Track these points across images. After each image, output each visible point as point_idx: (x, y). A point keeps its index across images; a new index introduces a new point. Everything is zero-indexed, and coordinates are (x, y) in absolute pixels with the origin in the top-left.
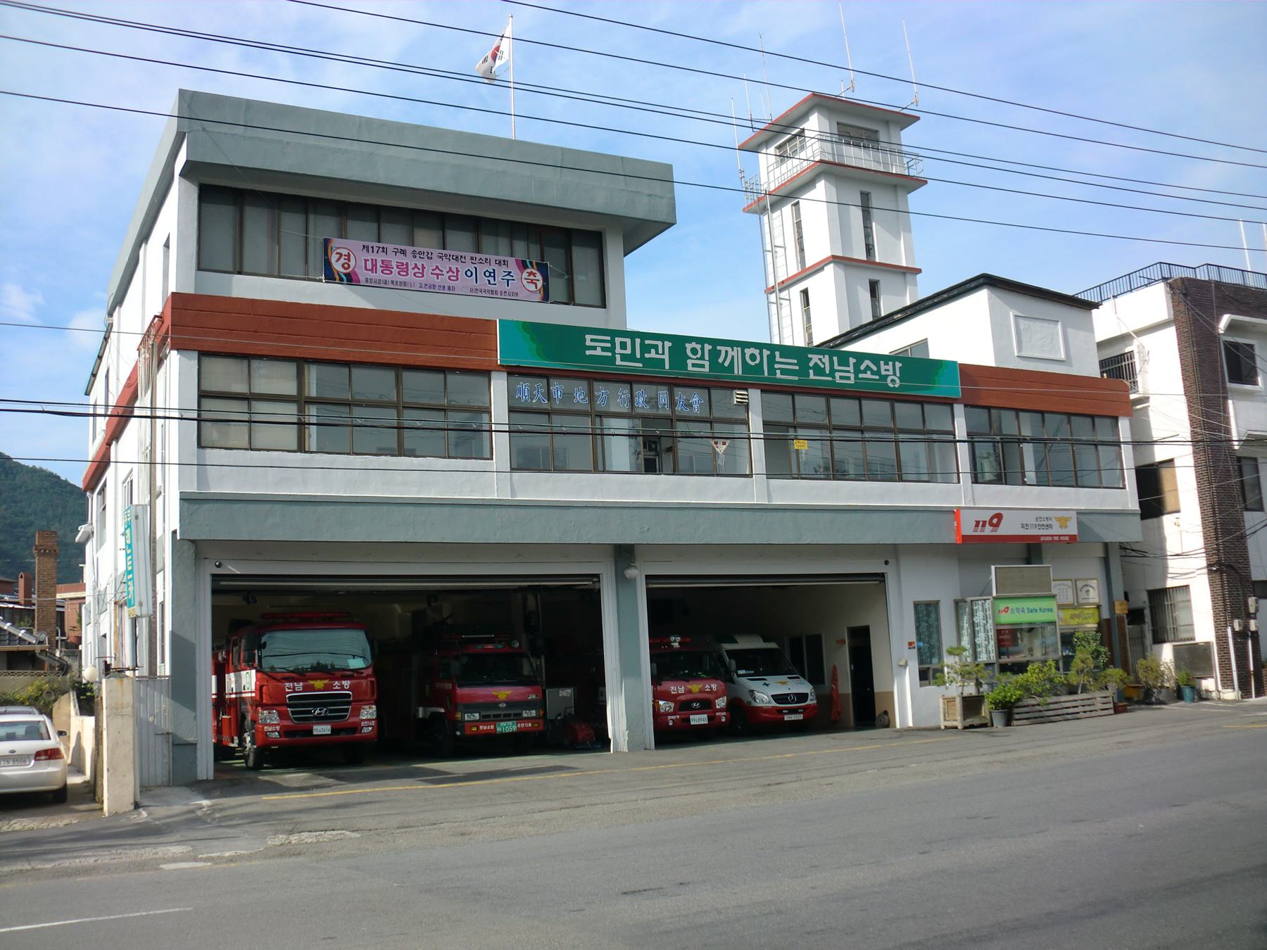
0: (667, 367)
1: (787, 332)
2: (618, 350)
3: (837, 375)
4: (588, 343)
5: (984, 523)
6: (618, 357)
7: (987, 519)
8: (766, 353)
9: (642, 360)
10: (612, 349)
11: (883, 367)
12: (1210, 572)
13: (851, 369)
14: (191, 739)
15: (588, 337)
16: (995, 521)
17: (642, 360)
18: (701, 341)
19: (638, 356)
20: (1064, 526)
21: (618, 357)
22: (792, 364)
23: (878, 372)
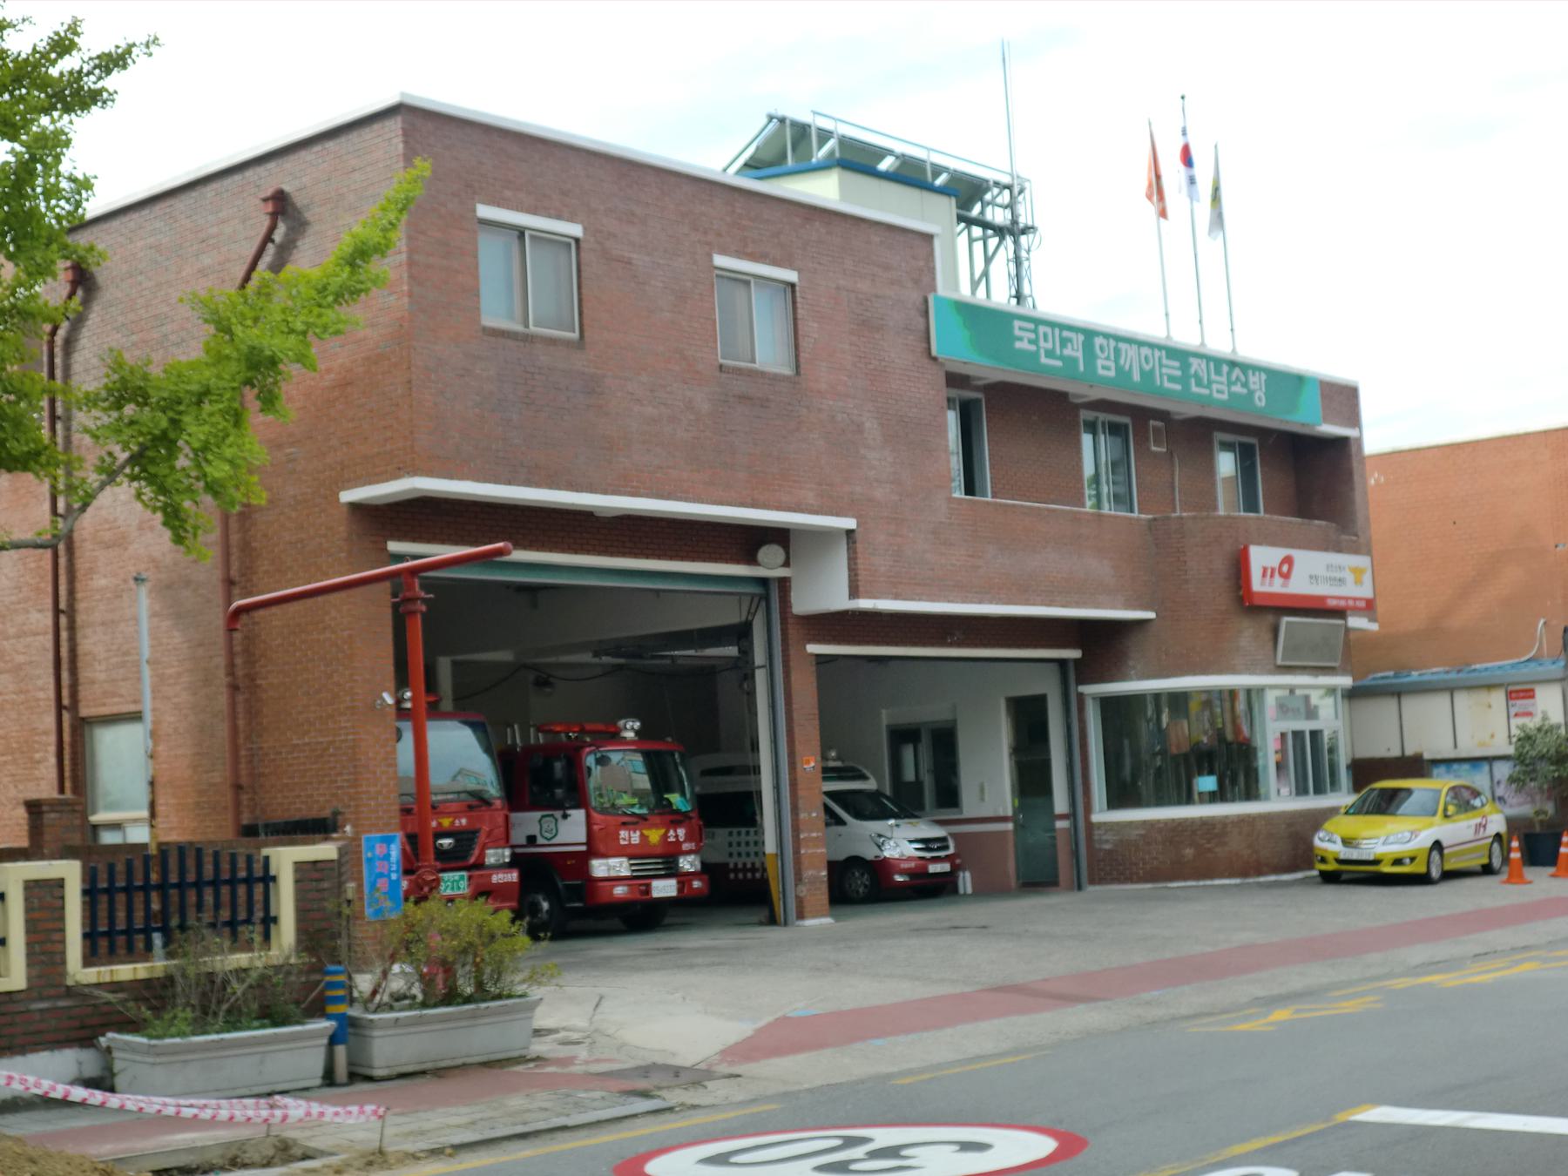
0: (1082, 368)
1: (956, 287)
2: (1042, 343)
3: (1215, 387)
4: (1017, 332)
5: (1273, 570)
6: (1042, 352)
7: (1276, 565)
8: (1112, 343)
9: (1061, 358)
10: (1035, 342)
11: (1252, 379)
12: (1255, 749)
13: (1224, 379)
14: (22, 813)
15: (1017, 323)
16: (1285, 568)
17: (1061, 358)
18: (1107, 336)
19: (1058, 352)
20: (1358, 582)
21: (1042, 352)
22: (1173, 368)
23: (1245, 385)
